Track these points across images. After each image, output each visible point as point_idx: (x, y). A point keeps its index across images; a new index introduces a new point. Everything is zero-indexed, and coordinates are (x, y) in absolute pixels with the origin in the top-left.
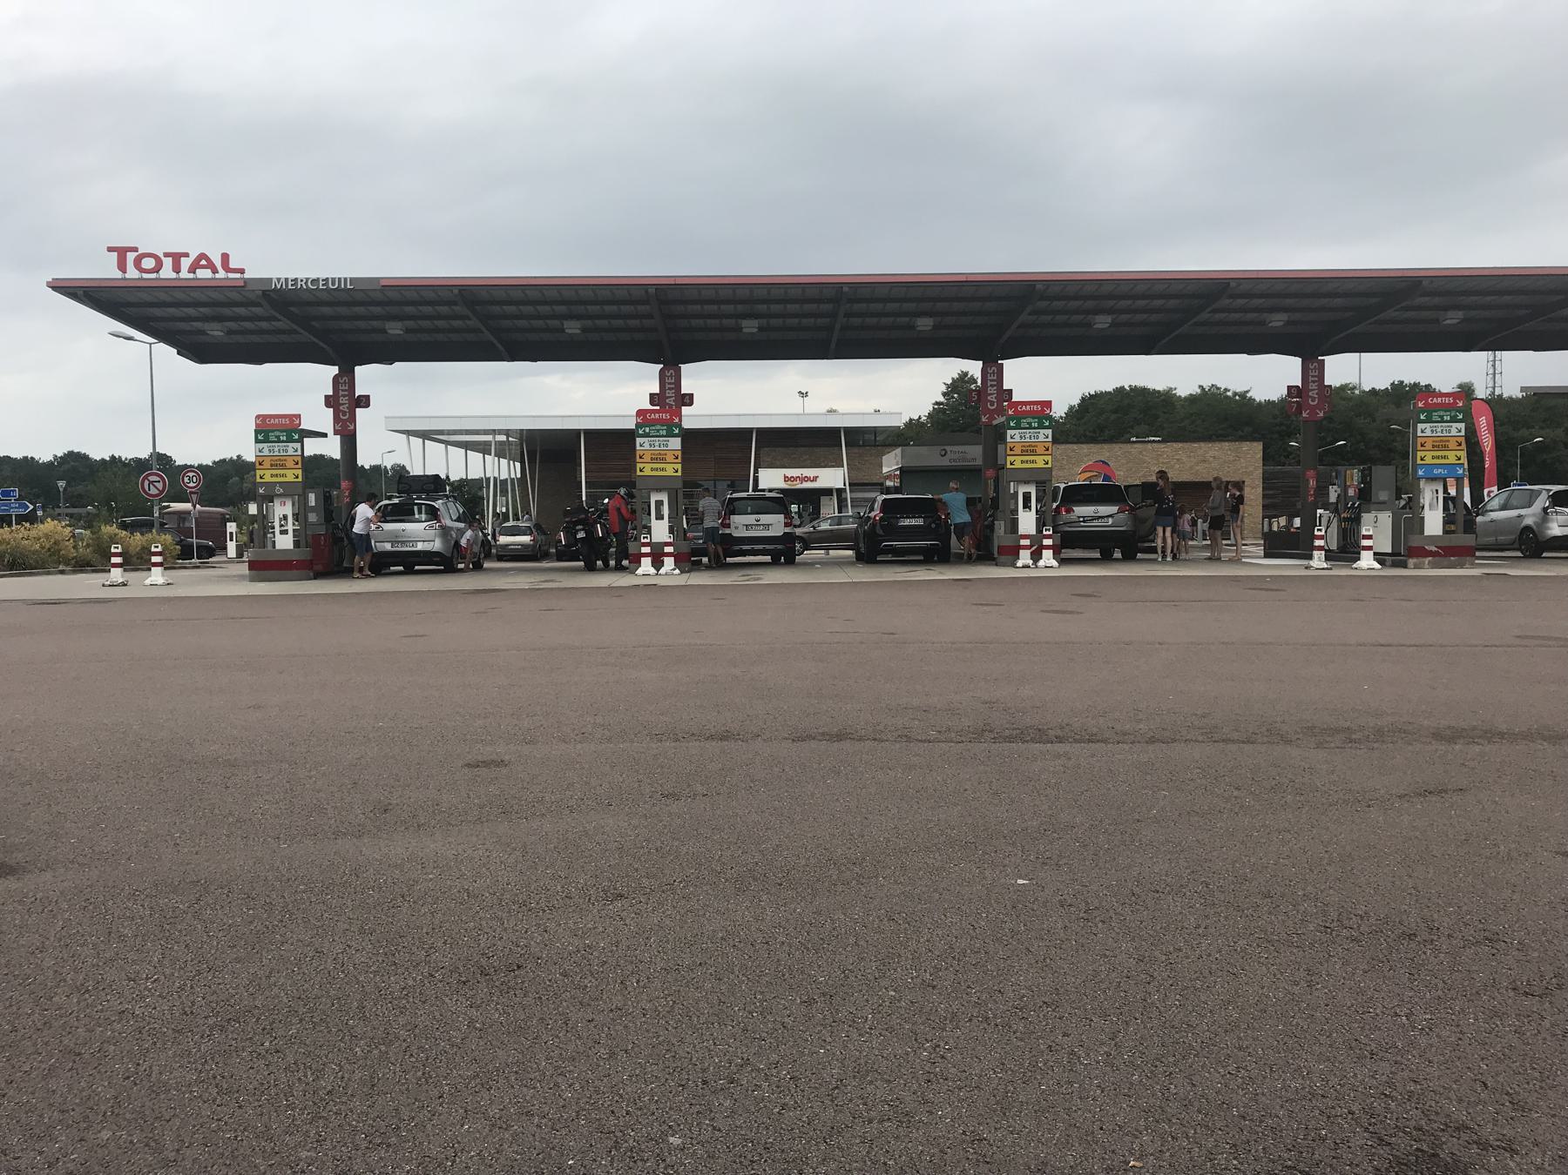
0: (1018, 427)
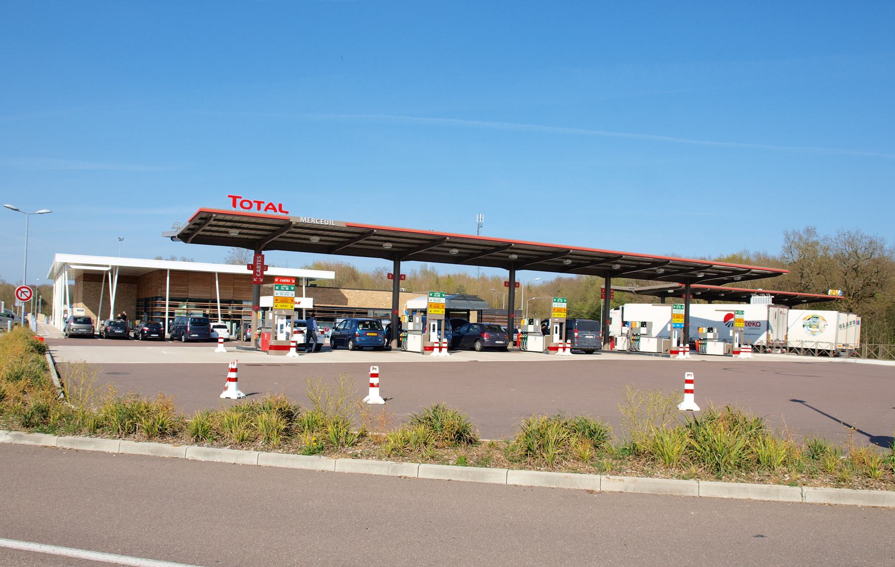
0: (279, 289)
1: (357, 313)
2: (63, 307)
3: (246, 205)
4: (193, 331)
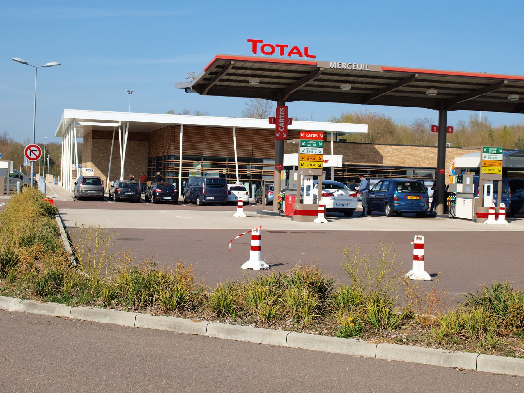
0: (306, 146)
1: (395, 173)
2: (72, 167)
3: (268, 49)
4: (209, 193)
